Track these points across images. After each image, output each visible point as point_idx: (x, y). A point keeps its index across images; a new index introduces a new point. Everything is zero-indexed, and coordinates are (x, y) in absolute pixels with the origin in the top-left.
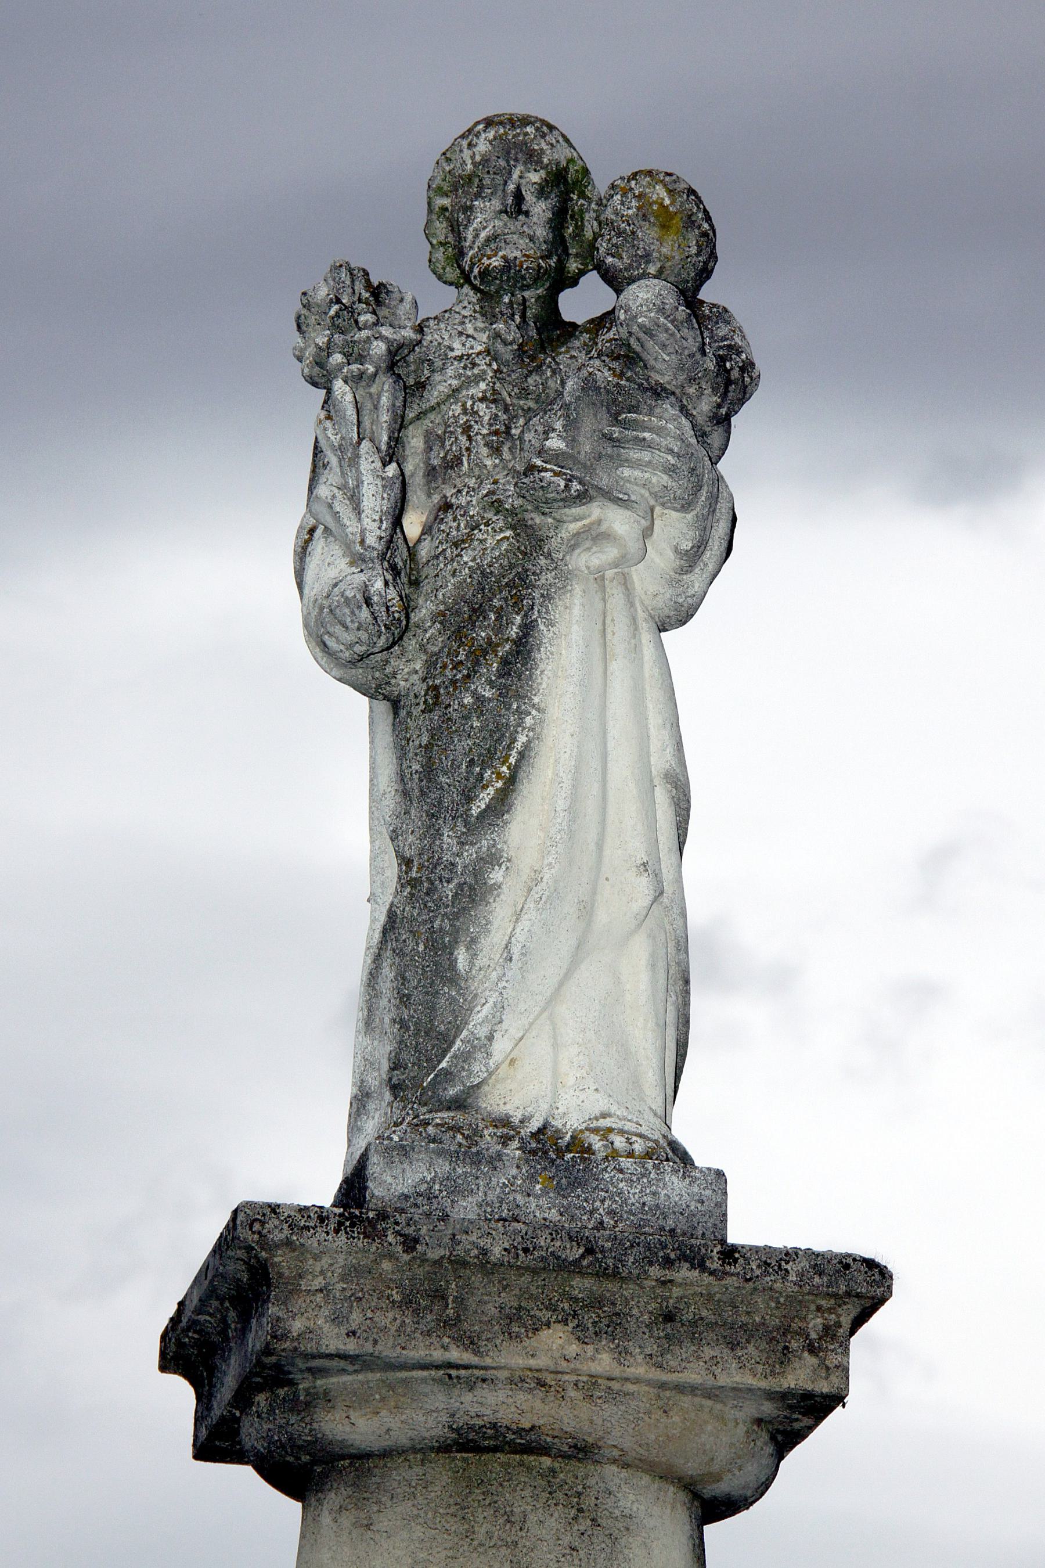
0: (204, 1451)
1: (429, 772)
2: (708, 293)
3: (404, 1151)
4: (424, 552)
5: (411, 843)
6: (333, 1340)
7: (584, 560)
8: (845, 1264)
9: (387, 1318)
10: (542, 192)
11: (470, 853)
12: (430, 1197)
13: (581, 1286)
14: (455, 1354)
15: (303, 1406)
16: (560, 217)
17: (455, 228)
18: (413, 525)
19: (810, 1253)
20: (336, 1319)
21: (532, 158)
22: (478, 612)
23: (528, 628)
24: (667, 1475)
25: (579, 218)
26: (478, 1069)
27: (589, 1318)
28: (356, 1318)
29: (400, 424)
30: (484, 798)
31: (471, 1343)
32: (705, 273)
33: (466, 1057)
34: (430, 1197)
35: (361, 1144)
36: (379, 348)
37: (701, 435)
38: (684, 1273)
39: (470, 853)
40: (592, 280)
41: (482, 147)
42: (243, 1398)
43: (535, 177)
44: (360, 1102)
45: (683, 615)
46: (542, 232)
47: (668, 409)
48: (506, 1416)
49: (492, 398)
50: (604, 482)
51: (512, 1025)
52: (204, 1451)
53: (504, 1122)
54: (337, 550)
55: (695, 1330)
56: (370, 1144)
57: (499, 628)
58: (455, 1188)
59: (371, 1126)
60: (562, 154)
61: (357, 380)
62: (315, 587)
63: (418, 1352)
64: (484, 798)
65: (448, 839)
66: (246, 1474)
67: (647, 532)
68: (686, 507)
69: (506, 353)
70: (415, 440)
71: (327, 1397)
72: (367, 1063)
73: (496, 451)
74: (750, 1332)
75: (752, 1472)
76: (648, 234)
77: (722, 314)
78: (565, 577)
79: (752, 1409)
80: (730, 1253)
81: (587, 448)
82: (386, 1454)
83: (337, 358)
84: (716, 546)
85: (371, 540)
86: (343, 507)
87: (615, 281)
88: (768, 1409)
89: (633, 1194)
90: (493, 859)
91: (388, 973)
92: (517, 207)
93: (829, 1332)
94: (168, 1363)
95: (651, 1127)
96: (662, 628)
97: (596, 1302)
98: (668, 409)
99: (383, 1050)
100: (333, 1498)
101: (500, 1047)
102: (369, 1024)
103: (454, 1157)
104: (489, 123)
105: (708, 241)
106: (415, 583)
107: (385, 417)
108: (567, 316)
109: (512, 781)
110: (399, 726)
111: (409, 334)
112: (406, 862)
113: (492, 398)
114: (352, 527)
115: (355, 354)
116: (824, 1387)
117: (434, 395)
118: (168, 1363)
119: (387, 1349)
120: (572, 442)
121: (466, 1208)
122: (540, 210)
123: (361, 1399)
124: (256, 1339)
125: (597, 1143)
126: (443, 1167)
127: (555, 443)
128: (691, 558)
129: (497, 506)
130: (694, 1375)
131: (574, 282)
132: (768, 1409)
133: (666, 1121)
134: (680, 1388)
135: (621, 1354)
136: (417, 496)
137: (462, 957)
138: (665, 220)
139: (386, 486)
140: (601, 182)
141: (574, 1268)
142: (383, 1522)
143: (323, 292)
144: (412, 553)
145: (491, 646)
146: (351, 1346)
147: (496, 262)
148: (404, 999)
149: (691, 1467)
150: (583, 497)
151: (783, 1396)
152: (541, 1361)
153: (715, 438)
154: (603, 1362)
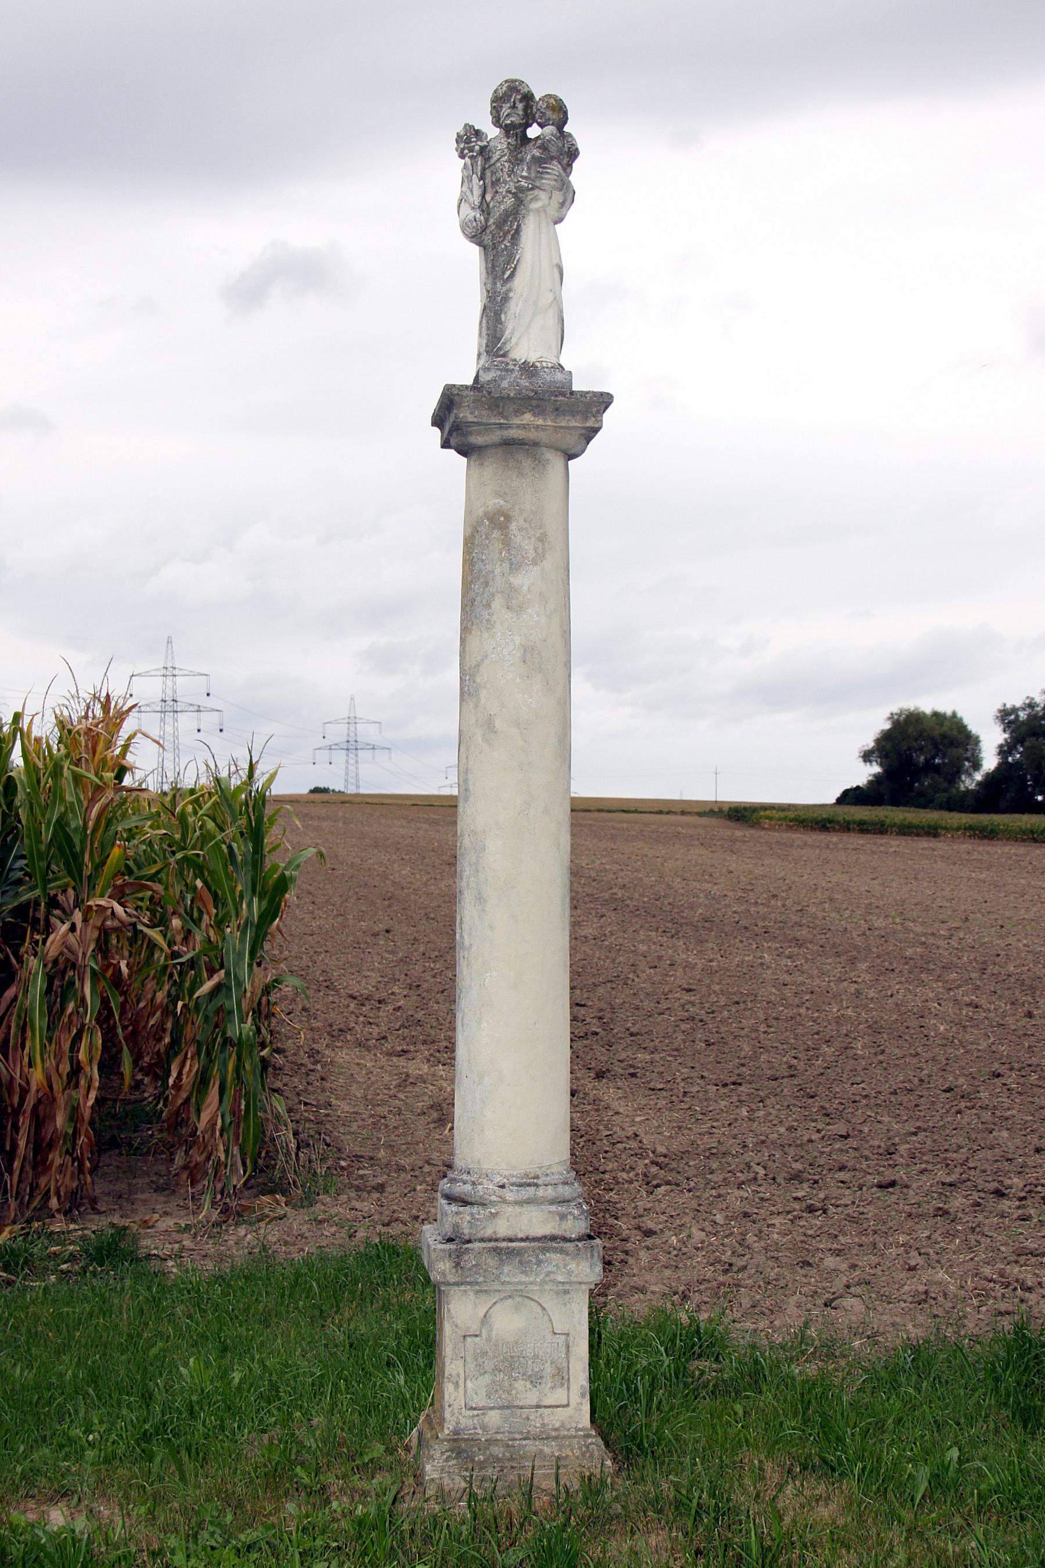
0: (443, 447)
1: (493, 267)
2: (566, 129)
3: (488, 369)
4: (491, 205)
5: (489, 286)
6: (471, 418)
7: (534, 206)
8: (602, 394)
9: (484, 413)
10: (521, 101)
11: (504, 289)
12: (495, 381)
13: (534, 403)
14: (502, 421)
15: (466, 435)
16: (525, 109)
17: (498, 112)
18: (488, 197)
19: (593, 392)
20: (471, 413)
21: (518, 91)
22: (505, 221)
23: (519, 226)
24: (557, 449)
25: (531, 107)
26: (508, 347)
27: (536, 411)
28: (476, 413)
29: (484, 169)
30: (508, 273)
31: (506, 418)
32: (565, 123)
33: (504, 343)
34: (495, 381)
35: (480, 366)
36: (477, 148)
37: (565, 170)
38: (561, 398)
39: (504, 289)
40: (535, 125)
41: (504, 89)
42: (450, 433)
43: (519, 97)
44: (479, 355)
45: (560, 220)
46: (521, 113)
47: (555, 162)
48: (515, 436)
49: (509, 161)
50: (538, 184)
51: (517, 335)
52: (443, 447)
53: (515, 360)
54: (467, 205)
55: (564, 413)
56: (199, 1121)
57: (511, 226)
58: (502, 378)
59: (482, 362)
60: (526, 90)
61: (471, 157)
62: (463, 217)
63: (493, 421)
64: (508, 273)
65: (499, 285)
66: (452, 452)
67: (550, 198)
68: (560, 190)
69: (512, 148)
70: (488, 174)
71: (471, 433)
72: (480, 345)
73: (509, 176)
74: (578, 412)
75: (580, 447)
76: (549, 113)
77: (570, 135)
78: (528, 211)
79: (579, 432)
80: (572, 393)
81: (533, 175)
82: (487, 446)
83: (466, 151)
84: (568, 203)
85: (476, 203)
86: (469, 193)
87: (541, 126)
88: (583, 431)
89: (548, 378)
90: (510, 290)
91: (484, 321)
92: (514, 107)
93: (598, 412)
94: (434, 424)
95: (554, 360)
96: (556, 223)
97: (538, 406)
98: (555, 162)
99: (484, 342)
100: (474, 458)
101: (514, 341)
102: (480, 335)
103: (501, 370)
104: (506, 81)
105: (565, 113)
106: (489, 214)
107: (479, 168)
108: (529, 136)
109: (515, 268)
110: (486, 254)
111: (485, 143)
112: (488, 291)
113: (509, 161)
114: (471, 199)
115: (471, 150)
116: (597, 426)
117: (493, 161)
118: (434, 424)
119: (484, 420)
120: (529, 173)
121: (505, 384)
122: (520, 106)
123: (479, 433)
124: (452, 419)
125: (538, 365)
126: (499, 373)
127: (525, 174)
128: (562, 204)
129: (510, 192)
130: (563, 424)
131: (531, 125)
132: (583, 431)
133: (558, 358)
134: (561, 427)
135: (545, 420)
136: (489, 189)
137: (503, 317)
138: (553, 109)
139: (480, 187)
140: (537, 97)
141: (531, 398)
142: (486, 464)
143: (462, 133)
144: (488, 205)
145: (509, 231)
146: (475, 420)
147: (509, 122)
148: (488, 329)
149: (564, 447)
150: (532, 189)
151: (586, 428)
152: (525, 422)
153: (568, 170)
154: (540, 422)
